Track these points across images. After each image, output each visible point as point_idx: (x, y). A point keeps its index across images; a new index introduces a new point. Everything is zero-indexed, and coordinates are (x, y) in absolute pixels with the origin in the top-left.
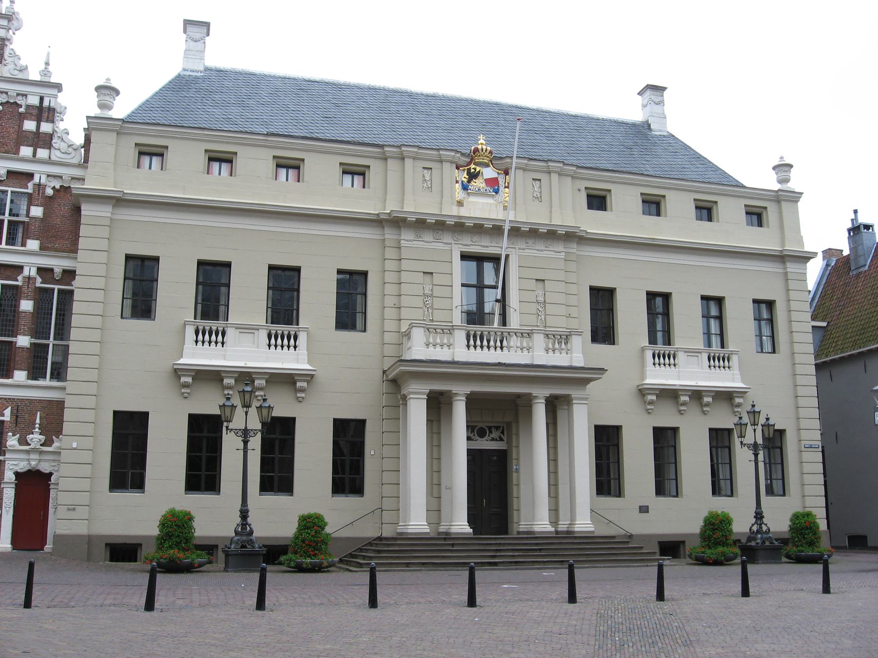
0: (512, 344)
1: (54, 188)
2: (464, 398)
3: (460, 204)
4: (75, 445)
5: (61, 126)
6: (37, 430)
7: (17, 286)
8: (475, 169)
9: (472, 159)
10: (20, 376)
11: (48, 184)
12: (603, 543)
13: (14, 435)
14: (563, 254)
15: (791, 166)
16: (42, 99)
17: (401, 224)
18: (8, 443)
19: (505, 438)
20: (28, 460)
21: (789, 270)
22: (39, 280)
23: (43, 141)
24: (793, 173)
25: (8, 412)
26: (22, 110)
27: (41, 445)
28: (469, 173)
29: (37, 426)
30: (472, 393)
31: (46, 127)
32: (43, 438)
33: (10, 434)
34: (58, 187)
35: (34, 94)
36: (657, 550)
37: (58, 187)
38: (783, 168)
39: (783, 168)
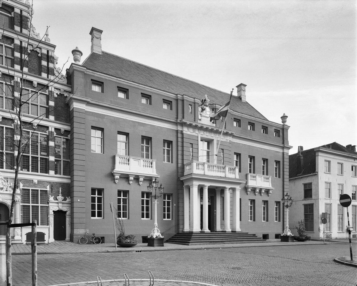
0: (214, 169)
1: (57, 94)
2: (197, 186)
3: (200, 120)
4: (79, 201)
5: (57, 66)
6: (60, 194)
7: (12, 129)
8: (204, 107)
9: (203, 103)
10: (52, 173)
11: (55, 92)
12: (243, 235)
13: (52, 196)
14: (229, 141)
15: (287, 117)
16: (48, 51)
17: (183, 125)
18: (50, 199)
19: (210, 201)
20: (58, 206)
21: (285, 152)
22: (55, 133)
23: (49, 71)
24: (288, 119)
25: (48, 187)
26: (39, 55)
27: (62, 200)
28: (202, 108)
29: (60, 193)
30: (210, 186)
31: (51, 65)
32: (63, 198)
33: (50, 196)
34: (58, 94)
35: (45, 48)
36: (262, 237)
37: (58, 94)
38: (284, 118)
39: (284, 118)
